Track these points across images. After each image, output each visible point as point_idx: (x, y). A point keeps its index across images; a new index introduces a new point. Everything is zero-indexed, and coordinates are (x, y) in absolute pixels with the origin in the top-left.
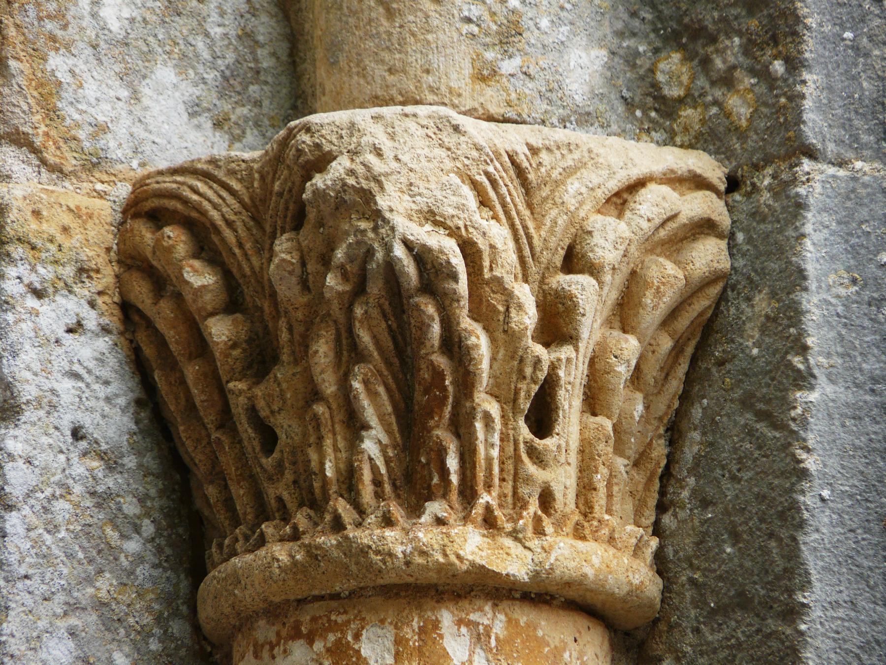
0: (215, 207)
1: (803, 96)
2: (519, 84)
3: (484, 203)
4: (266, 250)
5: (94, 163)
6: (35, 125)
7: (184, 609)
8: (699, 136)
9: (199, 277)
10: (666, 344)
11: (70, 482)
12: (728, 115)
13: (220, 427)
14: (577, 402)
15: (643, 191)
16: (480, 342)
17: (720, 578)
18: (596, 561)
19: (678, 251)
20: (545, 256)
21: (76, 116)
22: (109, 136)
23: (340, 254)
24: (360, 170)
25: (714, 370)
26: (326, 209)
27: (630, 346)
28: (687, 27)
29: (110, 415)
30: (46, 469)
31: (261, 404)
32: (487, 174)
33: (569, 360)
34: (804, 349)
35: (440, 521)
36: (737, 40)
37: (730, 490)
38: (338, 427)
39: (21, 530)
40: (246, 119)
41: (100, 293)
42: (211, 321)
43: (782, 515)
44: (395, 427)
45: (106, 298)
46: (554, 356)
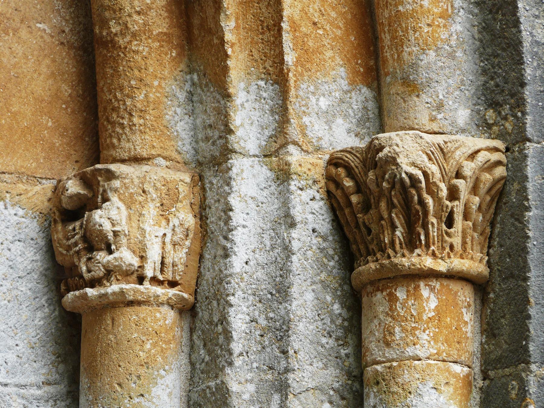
0: (353, 162)
1: (526, 123)
2: (443, 122)
3: (430, 159)
4: (366, 174)
5: (318, 149)
6: (299, 138)
7: (348, 282)
8: (498, 135)
9: (348, 183)
10: (488, 198)
11: (312, 245)
12: (506, 129)
13: (355, 228)
14: (461, 217)
15: (479, 153)
16: (430, 201)
17: (506, 269)
18: (467, 265)
19: (491, 171)
20: (450, 174)
21: (312, 135)
22: (322, 141)
23: (387, 176)
24: (392, 151)
25: (503, 206)
26: (383, 163)
27: (477, 200)
28: (494, 102)
29: (324, 224)
30: (304, 242)
31: (366, 221)
32: (431, 151)
33: (457, 205)
34: (528, 200)
35: (419, 255)
36: (508, 106)
37: (508, 242)
38: (389, 228)
39: (297, 261)
40: (365, 133)
41: (320, 188)
42: (352, 196)
43: (522, 250)
44: (406, 227)
45: (322, 190)
46: (452, 204)
